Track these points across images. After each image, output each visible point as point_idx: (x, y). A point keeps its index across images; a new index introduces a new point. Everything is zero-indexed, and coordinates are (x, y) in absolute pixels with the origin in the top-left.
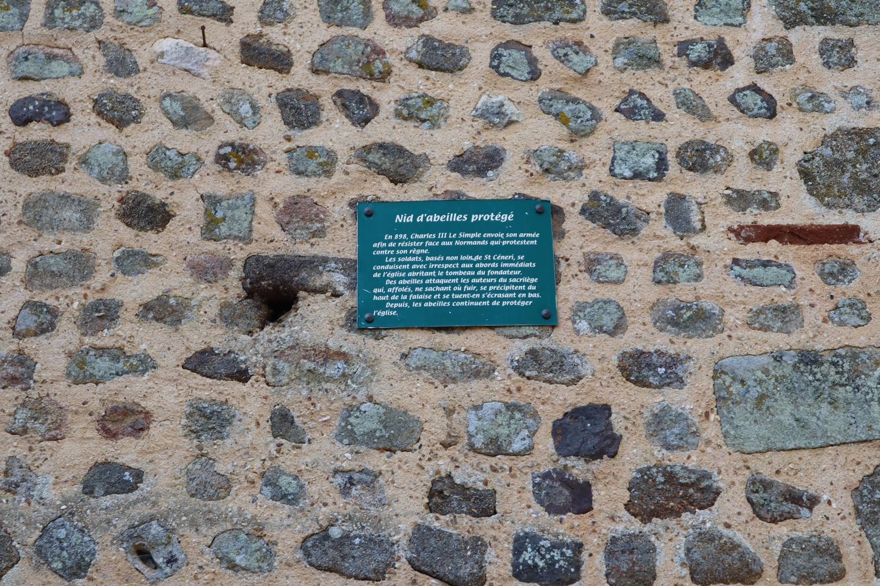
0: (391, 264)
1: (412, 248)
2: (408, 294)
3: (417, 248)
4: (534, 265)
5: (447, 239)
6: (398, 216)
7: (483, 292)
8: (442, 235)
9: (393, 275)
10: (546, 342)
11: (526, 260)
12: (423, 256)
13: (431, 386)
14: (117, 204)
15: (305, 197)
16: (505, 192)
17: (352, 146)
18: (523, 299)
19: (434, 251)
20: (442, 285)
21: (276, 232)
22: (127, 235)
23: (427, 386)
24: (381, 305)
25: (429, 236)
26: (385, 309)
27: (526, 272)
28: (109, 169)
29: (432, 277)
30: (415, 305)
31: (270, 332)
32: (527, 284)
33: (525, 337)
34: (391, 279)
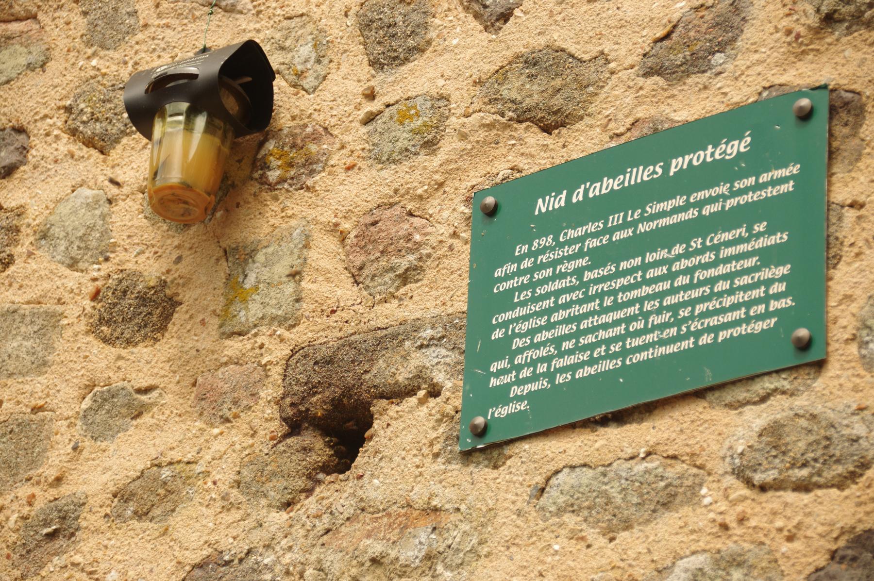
0: (523, 304)
1: (560, 261)
2: (548, 359)
3: (570, 258)
4: (785, 237)
5: (625, 225)
6: (540, 201)
7: (685, 320)
8: (615, 219)
9: (525, 327)
10: (801, 402)
11: (770, 232)
12: (579, 272)
13: (582, 545)
14: (88, 304)
15: (392, 205)
16: (742, 93)
17: (475, 77)
18: (760, 317)
19: (598, 257)
20: (608, 325)
21: (345, 292)
22: (101, 358)
23: (573, 546)
24: (502, 396)
25: (591, 228)
26: (506, 401)
27: (768, 257)
28: (81, 238)
29: (592, 313)
30: (560, 379)
31: (337, 495)
32: (769, 283)
33: (764, 399)
34: (521, 336)
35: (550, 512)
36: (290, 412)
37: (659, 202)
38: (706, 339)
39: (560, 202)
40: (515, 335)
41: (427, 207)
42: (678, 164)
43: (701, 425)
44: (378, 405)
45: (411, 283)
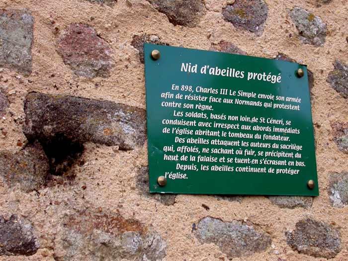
11: (293, 126)
19: (219, 108)
20: (225, 148)
24: (171, 167)
30: (203, 168)
34: (180, 137)
35: (203, 239)
36: (30, 131)
37: (244, 91)
38: (271, 171)
39: (194, 69)
40: (175, 135)
41: (109, 35)
42: (251, 76)
43: (269, 212)
44: (88, 146)
45: (100, 76)
